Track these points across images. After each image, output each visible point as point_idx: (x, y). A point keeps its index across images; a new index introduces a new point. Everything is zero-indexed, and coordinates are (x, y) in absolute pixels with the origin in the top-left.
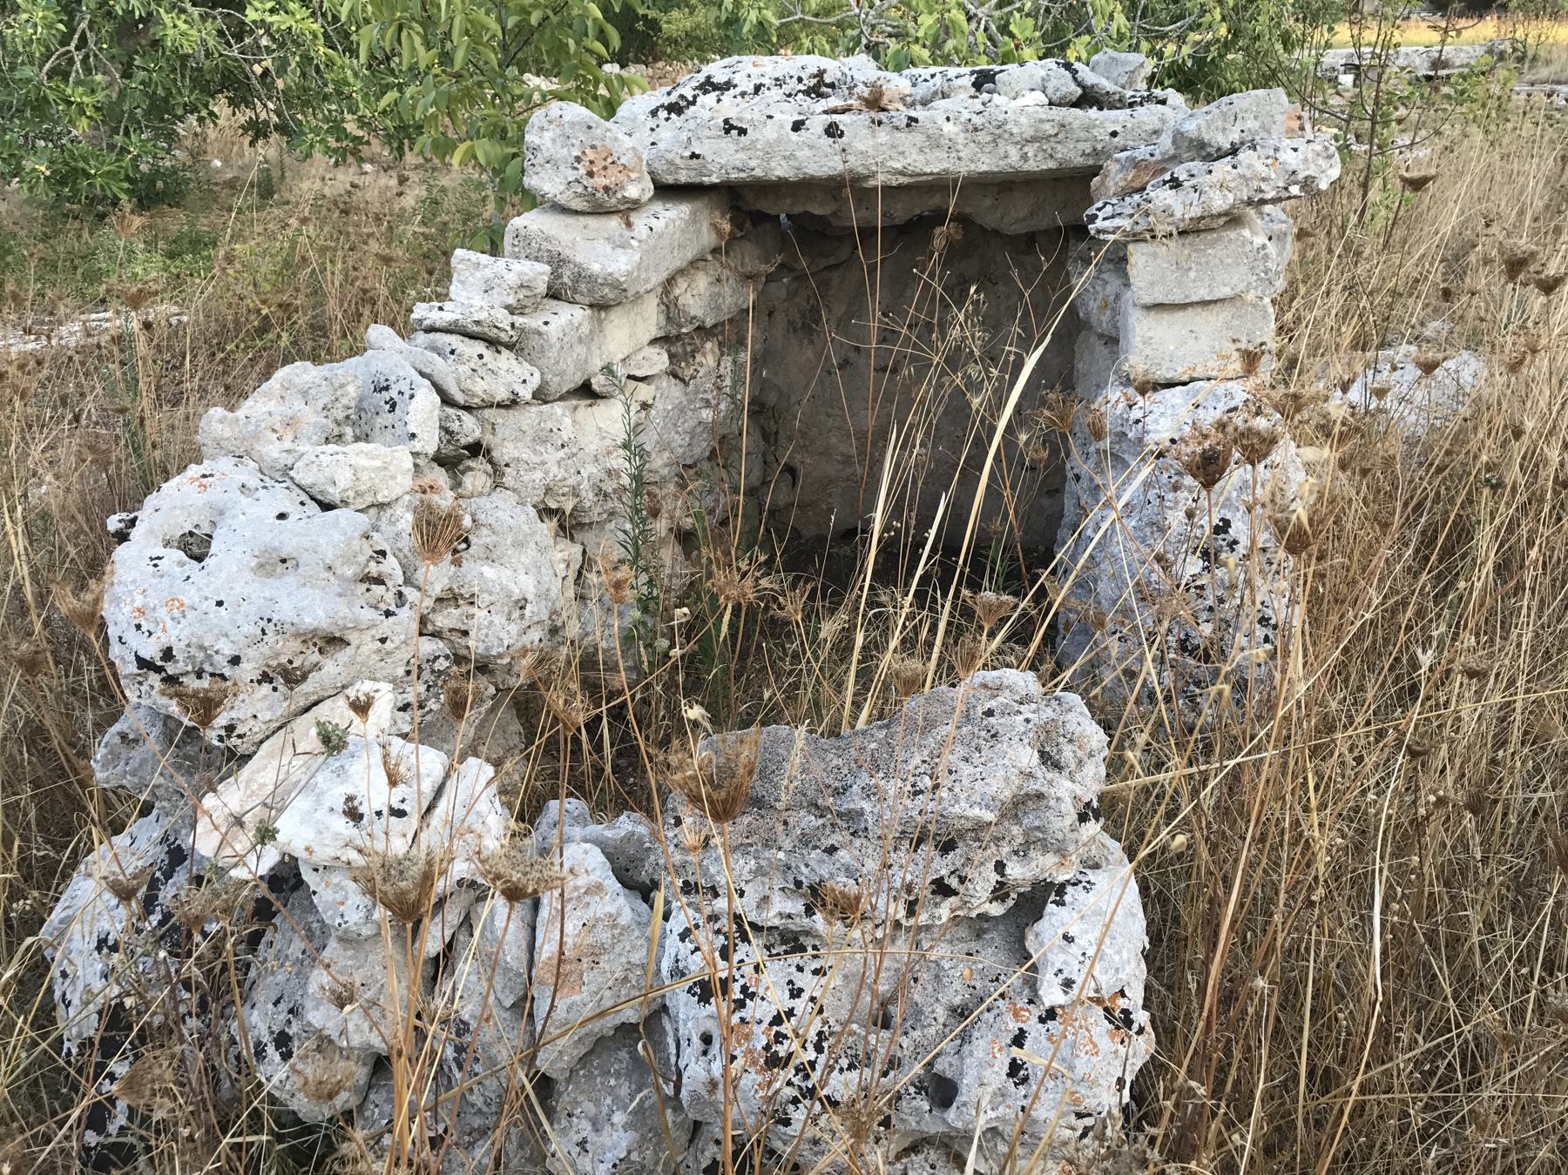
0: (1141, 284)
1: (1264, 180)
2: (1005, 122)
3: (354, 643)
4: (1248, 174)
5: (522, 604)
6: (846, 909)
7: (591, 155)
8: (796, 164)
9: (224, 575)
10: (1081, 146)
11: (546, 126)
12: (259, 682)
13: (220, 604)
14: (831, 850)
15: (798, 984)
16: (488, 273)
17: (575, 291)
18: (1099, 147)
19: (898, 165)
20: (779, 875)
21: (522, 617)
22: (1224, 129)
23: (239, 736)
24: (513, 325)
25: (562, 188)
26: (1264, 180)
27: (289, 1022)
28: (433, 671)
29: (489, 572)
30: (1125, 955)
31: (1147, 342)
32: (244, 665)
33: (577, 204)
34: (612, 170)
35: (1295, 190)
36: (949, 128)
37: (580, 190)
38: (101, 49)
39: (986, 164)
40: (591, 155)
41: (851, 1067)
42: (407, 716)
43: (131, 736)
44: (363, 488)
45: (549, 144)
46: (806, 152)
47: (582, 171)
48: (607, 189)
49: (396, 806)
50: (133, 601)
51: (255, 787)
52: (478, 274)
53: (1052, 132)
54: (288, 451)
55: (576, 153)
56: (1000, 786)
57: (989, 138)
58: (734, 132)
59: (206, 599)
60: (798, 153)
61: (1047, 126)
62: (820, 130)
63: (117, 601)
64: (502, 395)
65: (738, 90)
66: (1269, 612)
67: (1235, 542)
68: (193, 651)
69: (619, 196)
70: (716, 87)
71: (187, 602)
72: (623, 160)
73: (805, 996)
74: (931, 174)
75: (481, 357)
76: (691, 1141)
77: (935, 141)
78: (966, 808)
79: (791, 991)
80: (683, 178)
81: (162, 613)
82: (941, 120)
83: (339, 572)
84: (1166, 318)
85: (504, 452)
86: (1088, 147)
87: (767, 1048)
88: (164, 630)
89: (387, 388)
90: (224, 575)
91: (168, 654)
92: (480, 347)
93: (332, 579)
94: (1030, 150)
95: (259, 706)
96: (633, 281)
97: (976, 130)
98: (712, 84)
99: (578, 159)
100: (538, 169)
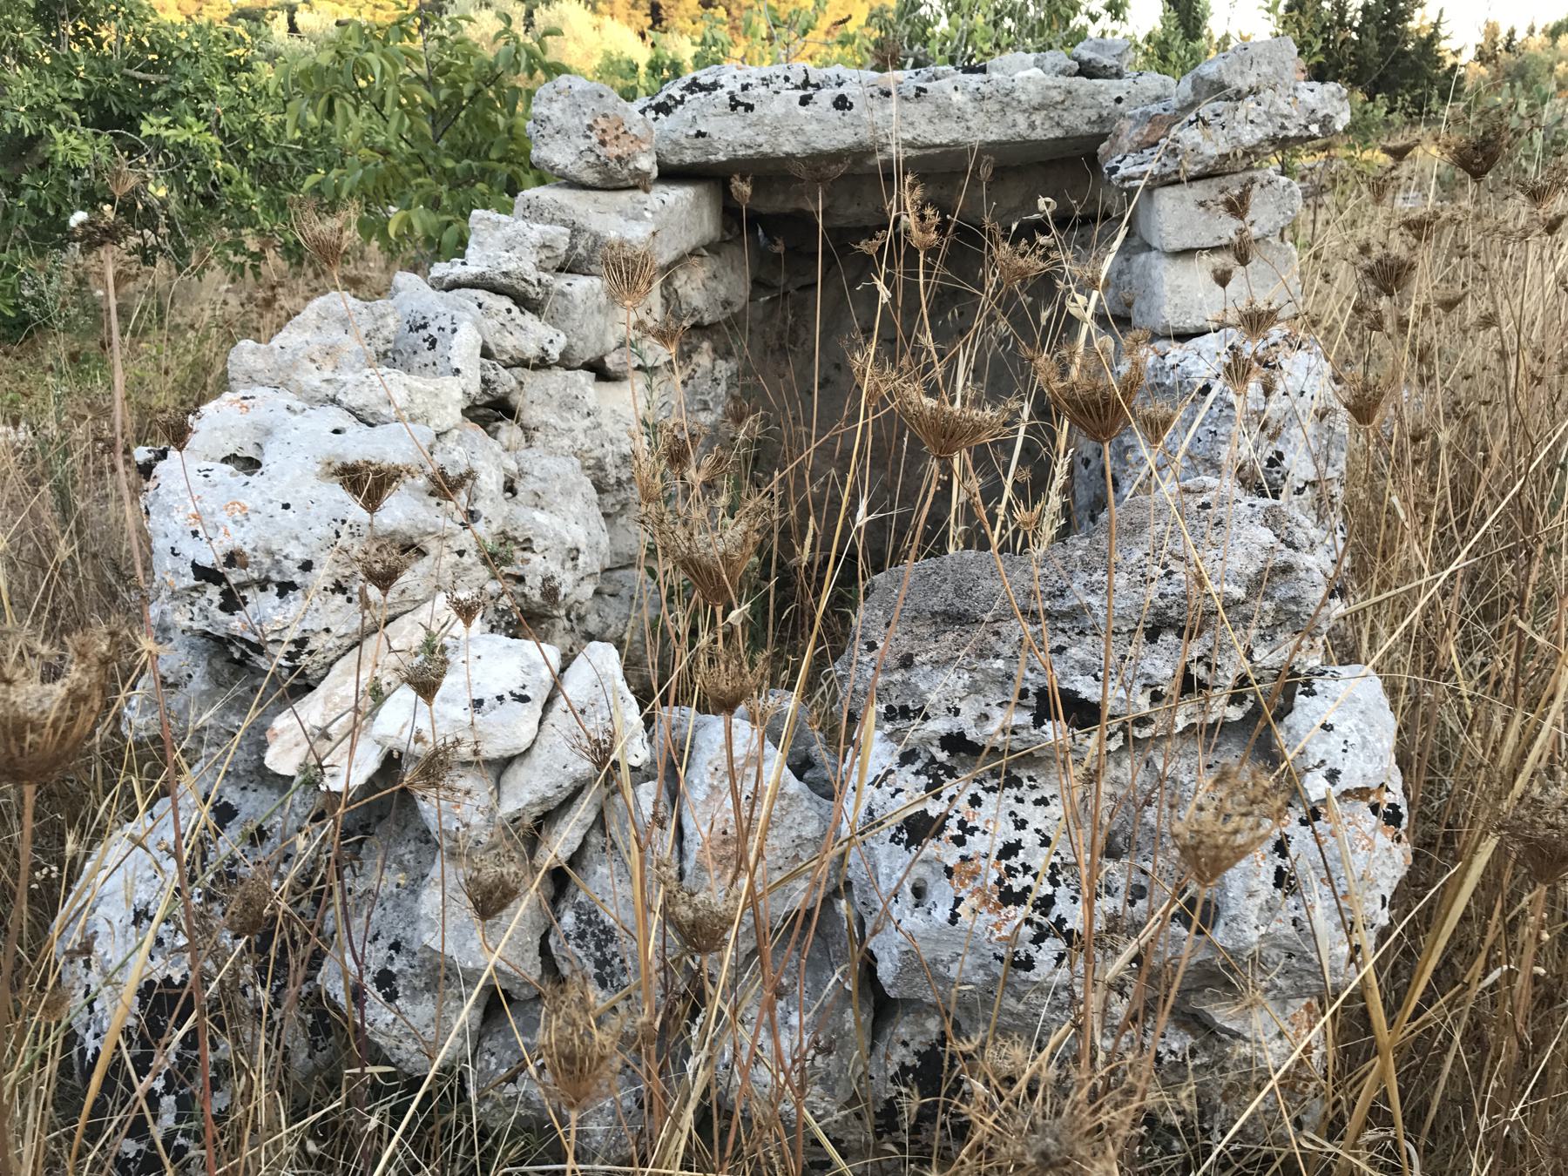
0: (1170, 229)
2: (1013, 90)
3: (433, 553)
6: (1083, 713)
7: (603, 124)
8: (804, 139)
9: (287, 478)
10: (1087, 113)
11: (555, 96)
12: (333, 591)
13: (286, 506)
14: (1060, 650)
15: (1021, 815)
16: (509, 231)
17: (591, 261)
18: (1105, 113)
19: (908, 137)
20: (996, 689)
21: (575, 567)
22: (1242, 73)
23: (311, 653)
24: (539, 281)
25: (573, 158)
26: (1286, 117)
27: (391, 958)
28: (497, 610)
29: (540, 517)
31: (1176, 290)
32: (316, 571)
33: (589, 176)
34: (624, 140)
35: (1314, 129)
36: (957, 98)
37: (592, 159)
40: (603, 124)
43: (170, 680)
45: (559, 114)
46: (815, 126)
47: (595, 140)
48: (619, 159)
49: (518, 692)
50: (187, 508)
51: (337, 700)
52: (498, 234)
53: (1059, 99)
54: (328, 381)
55: (588, 121)
58: (741, 109)
59: (271, 502)
60: (807, 128)
61: (1054, 93)
62: (829, 103)
63: (168, 510)
64: (532, 351)
69: (631, 166)
70: (702, 88)
71: (249, 505)
72: (634, 131)
73: (1030, 827)
74: (941, 145)
75: (509, 311)
76: (873, 1047)
77: (944, 112)
79: (1015, 822)
80: (688, 157)
81: (222, 517)
82: (949, 90)
85: (532, 415)
86: (1092, 114)
87: (1000, 882)
88: (226, 533)
89: (424, 326)
90: (287, 478)
92: (506, 303)
94: (1038, 118)
95: (333, 618)
98: (698, 85)
99: (590, 128)
100: (547, 140)
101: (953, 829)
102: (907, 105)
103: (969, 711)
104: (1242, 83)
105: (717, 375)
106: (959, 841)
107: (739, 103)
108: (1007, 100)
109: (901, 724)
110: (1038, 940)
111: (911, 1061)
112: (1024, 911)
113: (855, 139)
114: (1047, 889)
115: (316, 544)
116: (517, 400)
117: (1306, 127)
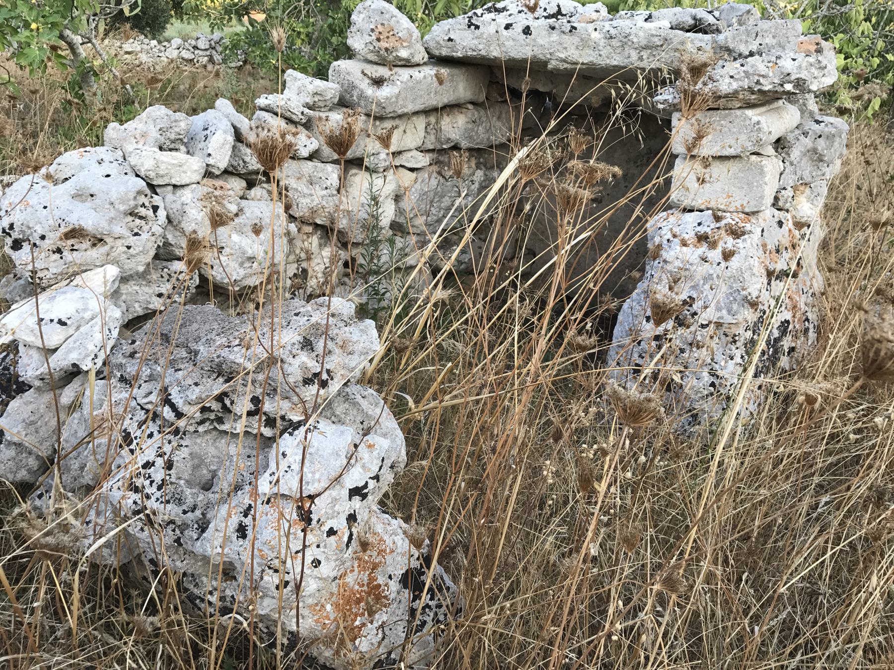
1: (763, 76)
2: (629, 35)
4: (751, 71)
5: (251, 259)
7: (380, 29)
12: (54, 252)
13: (45, 207)
19: (563, 56)
26: (763, 76)
29: (235, 237)
30: (317, 476)
32: (46, 241)
34: (392, 39)
36: (595, 35)
37: (372, 48)
38: (316, 6)
39: (616, 60)
40: (380, 29)
42: (161, 300)
44: (161, 173)
46: (511, 43)
47: (374, 37)
48: (387, 50)
53: (659, 43)
55: (373, 27)
57: (619, 44)
58: (473, 27)
60: (506, 43)
61: (656, 39)
62: (520, 30)
65: (509, 13)
68: (24, 228)
69: (394, 54)
71: (31, 203)
72: (400, 35)
77: (585, 43)
80: (444, 52)
83: (116, 207)
91: (11, 226)
93: (112, 210)
94: (645, 54)
96: (391, 104)
97: (611, 37)
99: (372, 30)
102: (564, 36)
104: (744, 49)
105: (475, 178)
107: (472, 24)
113: (532, 53)
115: (47, 228)
117: (782, 85)
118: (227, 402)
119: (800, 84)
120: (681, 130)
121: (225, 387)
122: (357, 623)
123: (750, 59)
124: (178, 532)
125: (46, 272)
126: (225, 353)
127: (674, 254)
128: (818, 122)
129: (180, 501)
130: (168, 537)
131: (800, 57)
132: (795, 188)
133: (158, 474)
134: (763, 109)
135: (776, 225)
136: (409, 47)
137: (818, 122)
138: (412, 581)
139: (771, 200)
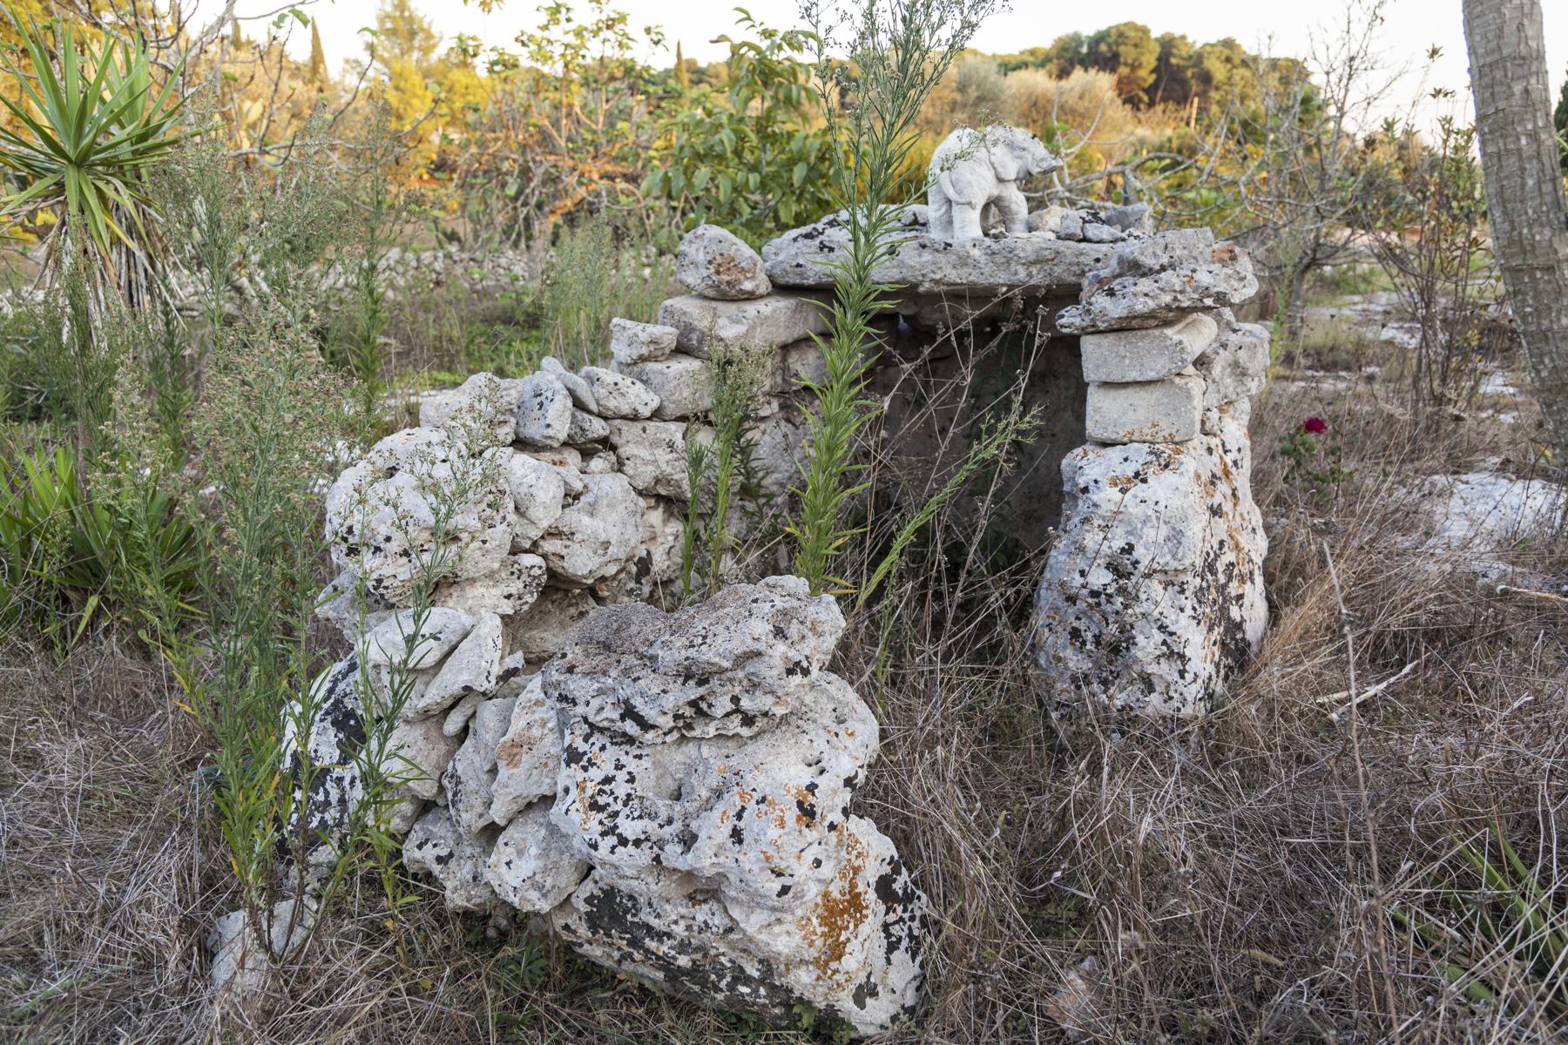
5: (606, 545)
7: (719, 259)
16: (630, 332)
19: (938, 277)
40: (719, 259)
41: (640, 817)
42: (510, 602)
48: (728, 283)
56: (739, 645)
66: (1167, 622)
67: (1137, 562)
77: (964, 261)
78: (708, 655)
80: (794, 280)
84: (1113, 393)
85: (624, 451)
94: (1034, 270)
101: (584, 762)
103: (595, 703)
106: (585, 769)
108: (1010, 257)
109: (564, 705)
110: (604, 834)
111: (596, 892)
112: (601, 816)
114: (618, 807)
116: (615, 439)
118: (704, 706)
119: (1221, 299)
120: (1096, 357)
121: (702, 691)
122: (842, 938)
123: (1163, 275)
124: (655, 849)
125: (391, 580)
126: (692, 652)
127: (1107, 496)
128: (1235, 331)
129: (653, 816)
130: (644, 856)
131: (1216, 267)
132: (1221, 410)
133: (621, 789)
134: (1180, 326)
135: (1205, 453)
136: (753, 278)
137: (1235, 331)
138: (884, 886)
139: (1198, 426)
